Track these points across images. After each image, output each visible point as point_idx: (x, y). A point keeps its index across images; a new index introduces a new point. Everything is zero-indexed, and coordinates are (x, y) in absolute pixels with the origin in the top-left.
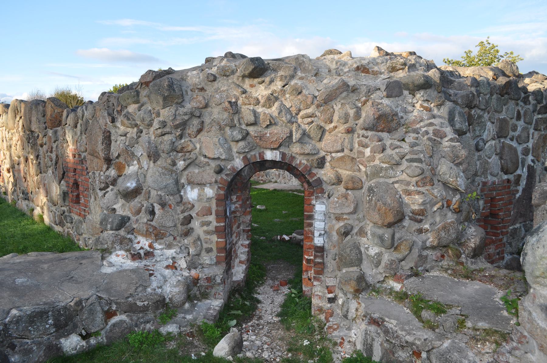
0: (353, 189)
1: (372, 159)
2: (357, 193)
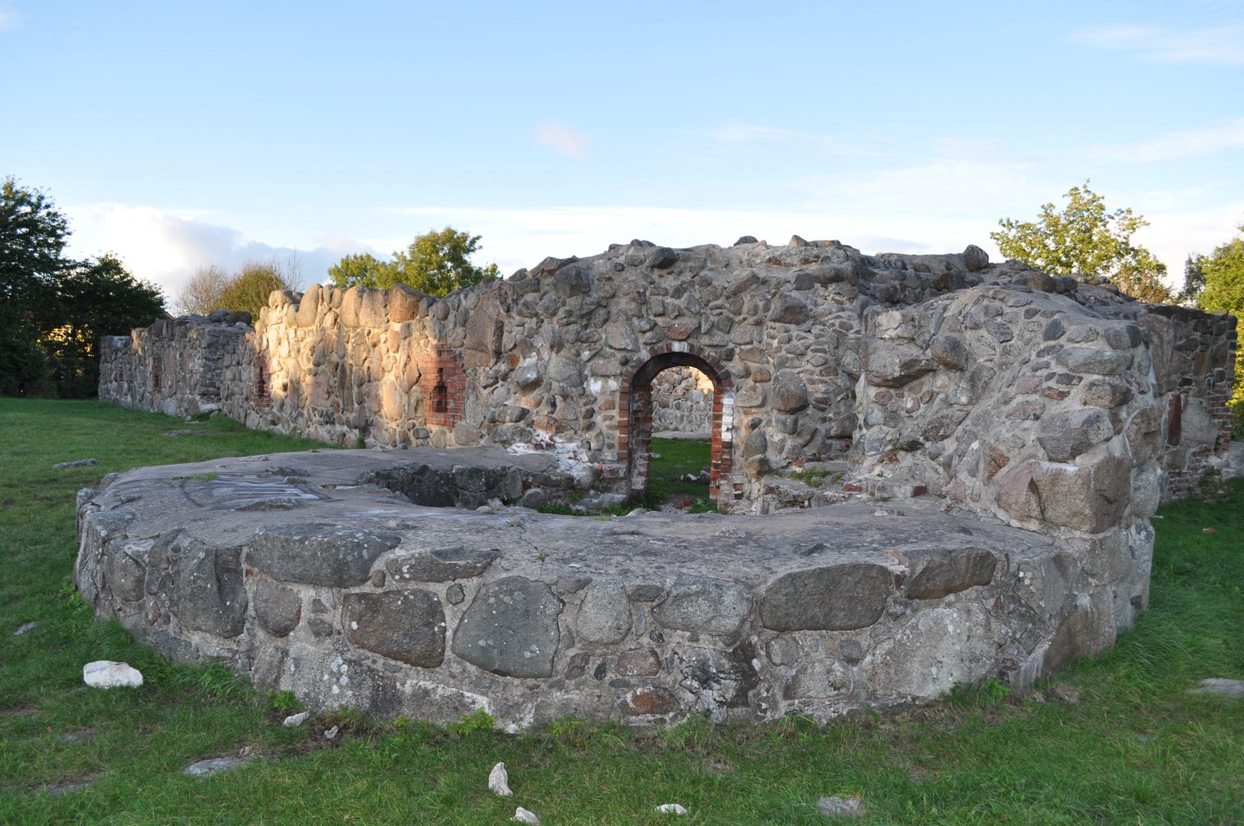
0: (762, 381)
1: (779, 349)
2: (766, 385)
